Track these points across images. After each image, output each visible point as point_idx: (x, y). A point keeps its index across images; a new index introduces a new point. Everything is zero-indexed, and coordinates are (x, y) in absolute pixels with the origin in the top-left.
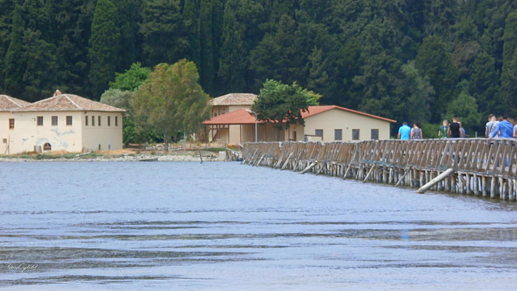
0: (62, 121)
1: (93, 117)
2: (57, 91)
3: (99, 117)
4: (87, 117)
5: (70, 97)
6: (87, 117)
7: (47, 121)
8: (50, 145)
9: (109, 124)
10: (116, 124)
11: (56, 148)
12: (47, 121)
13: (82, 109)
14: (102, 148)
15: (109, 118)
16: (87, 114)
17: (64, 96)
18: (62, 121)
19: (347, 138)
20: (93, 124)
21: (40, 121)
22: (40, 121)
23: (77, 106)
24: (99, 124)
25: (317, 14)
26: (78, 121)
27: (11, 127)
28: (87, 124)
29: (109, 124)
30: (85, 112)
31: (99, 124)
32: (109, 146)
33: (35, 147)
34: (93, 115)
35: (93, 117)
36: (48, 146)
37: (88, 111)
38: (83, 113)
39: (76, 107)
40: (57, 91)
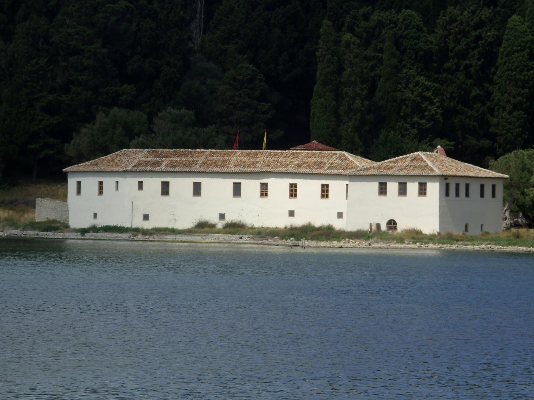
0: (413, 187)
1: (457, 185)
2: (439, 147)
3: (467, 186)
4: (447, 185)
5: (427, 156)
6: (447, 185)
7: (393, 187)
8: (395, 223)
9: (482, 195)
10: (494, 195)
11: (401, 226)
12: (393, 187)
13: (440, 173)
14: (469, 229)
15: (482, 186)
16: (447, 181)
17: (418, 155)
18: (413, 187)
19: (252, 186)
20: (457, 195)
21: (383, 190)
22: (383, 190)
23: (435, 169)
24: (467, 195)
25: (419, 74)
26: (434, 188)
27: (323, 196)
28: (447, 194)
29: (482, 195)
30: (446, 177)
31: (467, 195)
32: (101, 193)
33: (371, 225)
34: (494, 183)
35: (457, 185)
36: (392, 224)
37: (450, 176)
38: (443, 178)
39: (432, 170)
40: (439, 147)
